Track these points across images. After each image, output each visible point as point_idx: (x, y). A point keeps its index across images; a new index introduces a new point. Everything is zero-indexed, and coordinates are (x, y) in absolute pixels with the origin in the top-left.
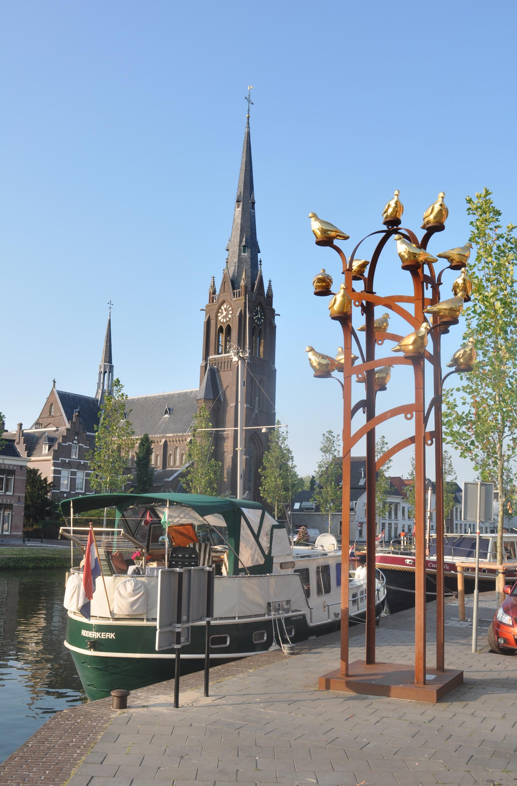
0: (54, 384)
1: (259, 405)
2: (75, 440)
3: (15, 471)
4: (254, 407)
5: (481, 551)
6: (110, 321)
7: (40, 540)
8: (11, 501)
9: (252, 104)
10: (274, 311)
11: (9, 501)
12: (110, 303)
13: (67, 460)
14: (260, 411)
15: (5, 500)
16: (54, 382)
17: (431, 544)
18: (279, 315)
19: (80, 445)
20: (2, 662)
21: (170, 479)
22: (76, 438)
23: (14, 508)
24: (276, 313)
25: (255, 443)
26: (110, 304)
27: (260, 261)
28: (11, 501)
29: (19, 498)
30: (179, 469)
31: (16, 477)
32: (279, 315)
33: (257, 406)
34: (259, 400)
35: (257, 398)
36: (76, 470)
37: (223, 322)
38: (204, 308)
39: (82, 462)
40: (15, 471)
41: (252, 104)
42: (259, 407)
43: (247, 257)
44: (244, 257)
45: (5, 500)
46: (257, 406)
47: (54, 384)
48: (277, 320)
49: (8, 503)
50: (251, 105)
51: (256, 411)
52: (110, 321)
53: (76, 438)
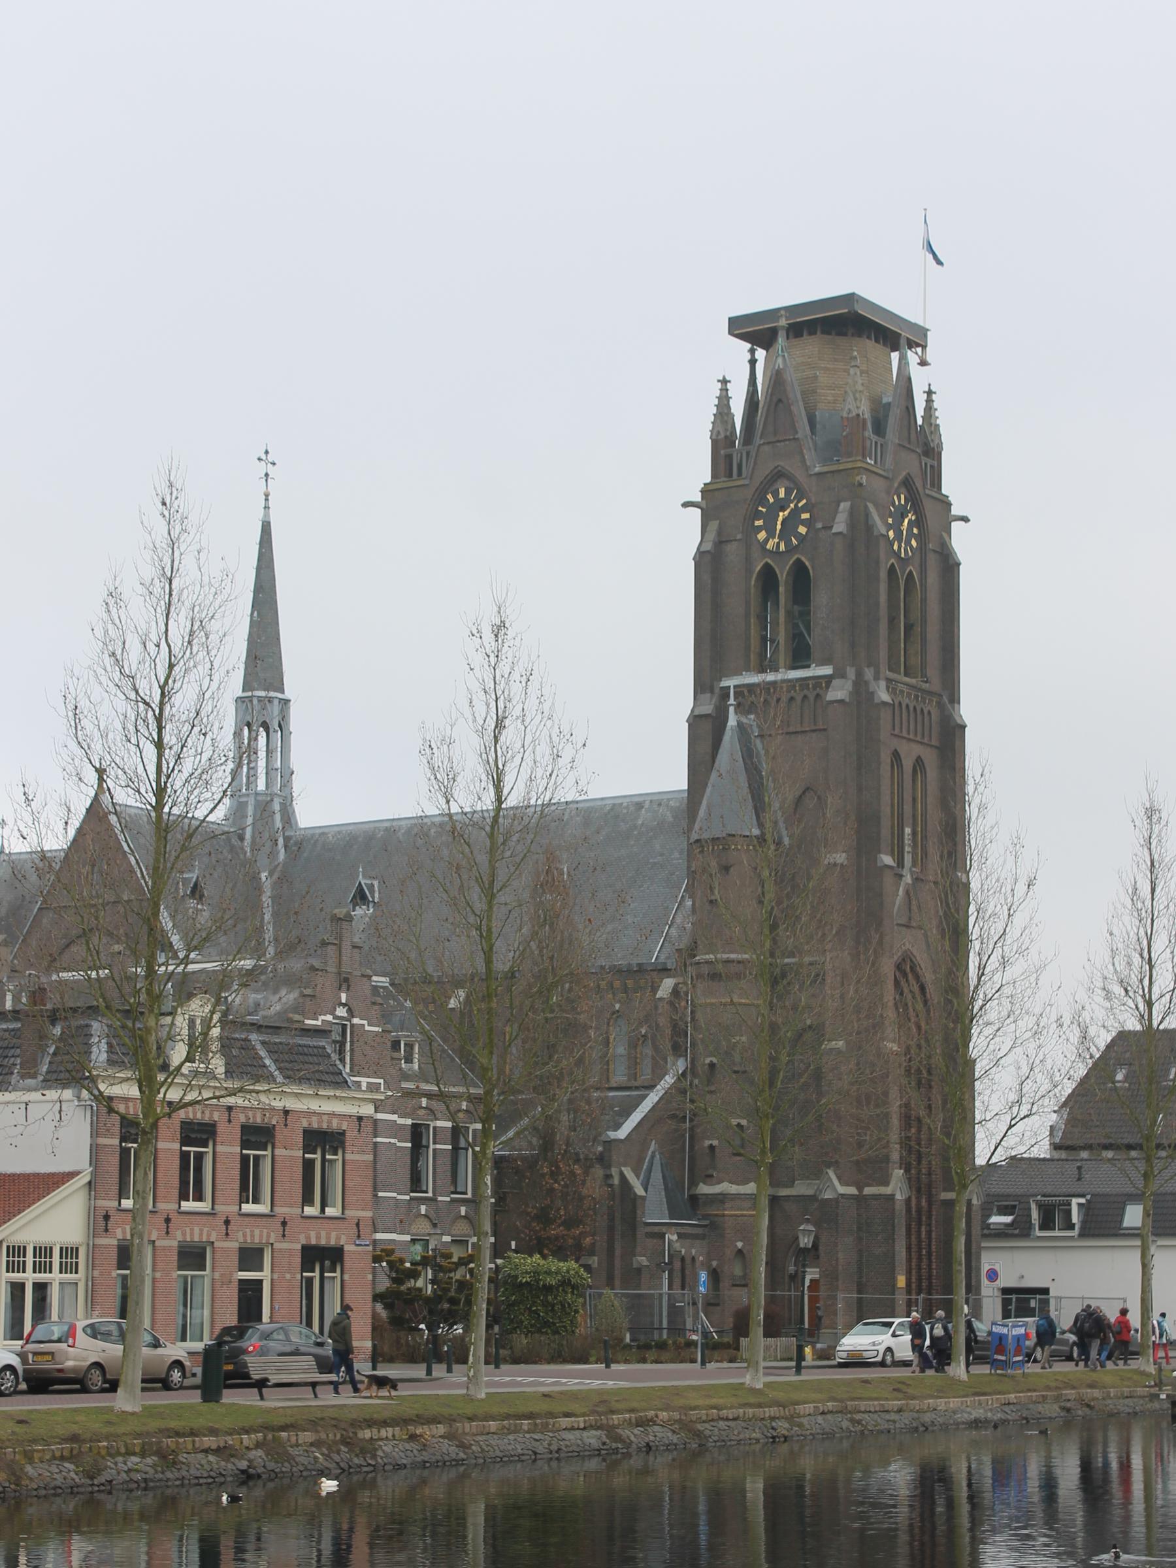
1: (914, 854)
3: (343, 1133)
5: (593, 1359)
6: (266, 529)
8: (338, 1238)
14: (917, 880)
18: (965, 519)
19: (356, 1021)
21: (622, 1133)
22: (343, 997)
23: (347, 1259)
24: (955, 511)
28: (338, 1238)
29: (358, 1225)
30: (348, 1067)
31: (348, 1156)
32: (965, 519)
34: (914, 833)
35: (908, 830)
37: (776, 553)
38: (698, 498)
40: (343, 1133)
45: (313, 1234)
48: (960, 539)
49: (333, 1242)
52: (266, 529)
53: (343, 997)
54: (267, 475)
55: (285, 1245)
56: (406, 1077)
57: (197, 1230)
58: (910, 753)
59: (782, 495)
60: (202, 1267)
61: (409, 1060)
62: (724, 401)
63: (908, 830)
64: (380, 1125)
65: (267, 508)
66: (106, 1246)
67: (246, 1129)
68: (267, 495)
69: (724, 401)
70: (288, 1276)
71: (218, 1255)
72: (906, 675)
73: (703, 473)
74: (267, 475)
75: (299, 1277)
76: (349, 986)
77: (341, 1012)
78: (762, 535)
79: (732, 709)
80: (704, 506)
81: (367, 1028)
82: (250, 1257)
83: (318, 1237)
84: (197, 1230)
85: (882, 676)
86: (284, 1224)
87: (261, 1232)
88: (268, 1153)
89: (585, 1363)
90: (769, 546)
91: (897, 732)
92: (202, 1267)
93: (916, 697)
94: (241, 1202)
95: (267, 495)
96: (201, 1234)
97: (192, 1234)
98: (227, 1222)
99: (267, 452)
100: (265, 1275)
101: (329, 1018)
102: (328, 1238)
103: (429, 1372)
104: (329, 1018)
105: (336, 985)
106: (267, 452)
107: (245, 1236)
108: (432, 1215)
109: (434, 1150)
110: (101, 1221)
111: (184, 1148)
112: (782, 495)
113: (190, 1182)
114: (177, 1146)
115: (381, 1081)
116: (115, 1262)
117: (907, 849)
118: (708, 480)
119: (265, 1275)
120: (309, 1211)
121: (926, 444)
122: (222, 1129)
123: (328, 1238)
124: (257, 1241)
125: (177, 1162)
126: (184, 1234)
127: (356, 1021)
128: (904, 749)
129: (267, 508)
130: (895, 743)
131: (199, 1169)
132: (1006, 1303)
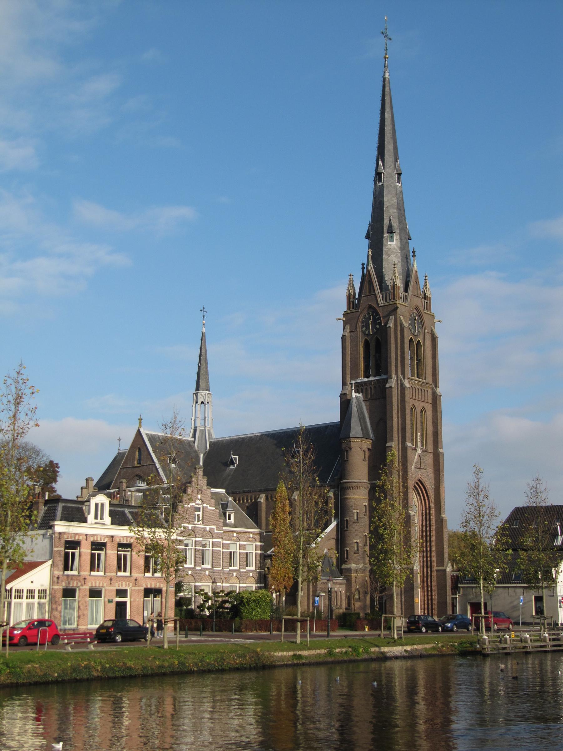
0: (140, 423)
1: (422, 442)
2: (198, 499)
4: (417, 446)
7: (199, 633)
9: (390, 39)
10: (433, 316)
11: (158, 584)
12: (203, 310)
13: (190, 526)
14: (423, 451)
15: (153, 583)
16: (140, 420)
17: (80, 599)
19: (205, 505)
20: (424, 745)
25: (419, 493)
26: (204, 311)
27: (414, 252)
28: (160, 585)
33: (419, 444)
34: (422, 435)
35: (419, 434)
36: (245, 543)
39: (208, 528)
41: (390, 39)
42: (422, 445)
43: (396, 247)
44: (392, 247)
45: (153, 583)
46: (419, 444)
47: (140, 423)
50: (388, 41)
51: (419, 451)
53: (199, 497)
54: (204, 316)
55: (136, 588)
56: (226, 525)
57: (97, 583)
58: (419, 406)
60: (101, 597)
61: (229, 519)
62: (351, 283)
63: (419, 434)
64: (214, 543)
66: (86, 589)
67: (93, 544)
69: (351, 283)
70: (137, 600)
71: (107, 591)
72: (418, 377)
73: (345, 309)
74: (204, 316)
75: (142, 600)
77: (199, 502)
80: (344, 319)
81: (209, 508)
82: (121, 593)
83: (151, 585)
84: (97, 583)
85: (406, 377)
86: (136, 580)
87: (126, 583)
88: (104, 552)
89: (356, 630)
91: (414, 397)
92: (101, 597)
93: (422, 385)
94: (145, 573)
96: (99, 584)
97: (95, 584)
98: (111, 579)
99: (204, 308)
100: (128, 600)
102: (155, 585)
103: (328, 633)
104: (193, 504)
106: (204, 308)
107: (118, 584)
108: (238, 576)
109: (213, 550)
110: (55, 580)
111: (147, 554)
113: (94, 564)
114: (89, 551)
115: (215, 527)
116: (88, 595)
117: (419, 440)
118: (346, 310)
119: (128, 600)
120: (147, 575)
121: (425, 295)
122: (108, 545)
123: (155, 585)
124: (97, 586)
125: (89, 557)
126: (92, 584)
127: (205, 505)
130: (412, 402)
131: (99, 559)
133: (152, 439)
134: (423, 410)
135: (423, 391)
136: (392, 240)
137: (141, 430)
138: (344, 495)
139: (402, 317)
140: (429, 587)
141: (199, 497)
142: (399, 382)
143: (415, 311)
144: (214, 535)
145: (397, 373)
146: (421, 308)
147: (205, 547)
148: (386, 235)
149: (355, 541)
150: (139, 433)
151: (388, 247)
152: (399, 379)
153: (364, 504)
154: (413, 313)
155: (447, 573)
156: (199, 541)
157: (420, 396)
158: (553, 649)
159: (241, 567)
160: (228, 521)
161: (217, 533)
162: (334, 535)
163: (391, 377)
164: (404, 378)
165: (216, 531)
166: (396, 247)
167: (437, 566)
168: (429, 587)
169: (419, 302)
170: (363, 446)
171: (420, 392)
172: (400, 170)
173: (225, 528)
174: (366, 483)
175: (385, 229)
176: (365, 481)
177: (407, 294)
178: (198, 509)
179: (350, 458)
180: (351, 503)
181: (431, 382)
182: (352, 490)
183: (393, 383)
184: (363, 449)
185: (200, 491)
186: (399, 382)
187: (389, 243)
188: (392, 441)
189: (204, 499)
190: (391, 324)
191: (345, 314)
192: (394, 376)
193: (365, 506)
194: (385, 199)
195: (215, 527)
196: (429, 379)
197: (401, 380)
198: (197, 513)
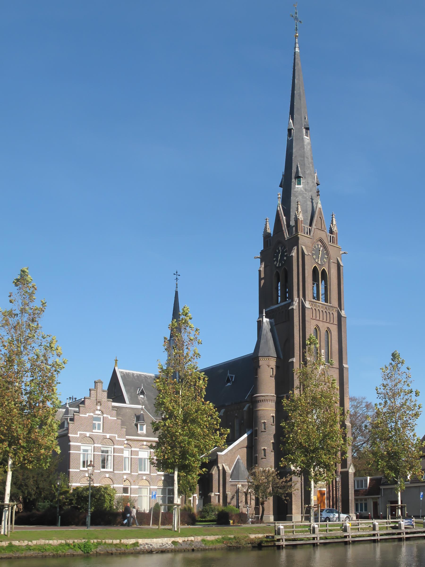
0: (116, 363)
6: (177, 293)
19: (105, 415)
39: (108, 436)
47: (116, 363)
52: (177, 293)
54: (177, 278)
59: (325, 260)
64: (115, 450)
65: (177, 287)
68: (177, 284)
73: (262, 248)
74: (177, 278)
76: (101, 404)
78: (275, 263)
79: (264, 316)
81: (109, 416)
90: (277, 265)
93: (326, 308)
95: (177, 284)
99: (177, 272)
101: (92, 414)
104: (92, 414)
105: (95, 403)
106: (177, 272)
112: (325, 260)
115: (116, 435)
127: (105, 415)
128: (320, 324)
129: (177, 287)
132: (155, 524)
133: (124, 376)
134: (328, 331)
135: (332, 315)
136: (299, 184)
137: (116, 368)
138: (256, 407)
139: (303, 247)
140: (334, 486)
141: (99, 408)
142: (301, 305)
143: (320, 243)
144: (115, 442)
145: (298, 297)
146: (326, 241)
147: (108, 453)
148: (293, 180)
149: (263, 448)
150: (114, 372)
151: (296, 190)
152: (301, 301)
153: (272, 415)
154: (318, 245)
155: (350, 474)
156: (98, 447)
157: (325, 318)
158: (322, 541)
159: (151, 471)
160: (139, 432)
161: (118, 440)
162: (246, 444)
163: (292, 300)
164: (305, 301)
165: (117, 439)
166: (302, 189)
167: (341, 468)
168: (334, 486)
169: (325, 235)
170: (270, 364)
171: (325, 314)
172: (308, 125)
173: (127, 437)
174: (273, 396)
175: (293, 175)
176: (272, 395)
177: (310, 228)
178: (98, 419)
179: (259, 374)
180: (260, 413)
181: (337, 305)
182: (260, 403)
183: (295, 305)
184: (271, 367)
185: (99, 402)
186: (301, 305)
187: (297, 186)
188: (293, 357)
189: (103, 410)
190: (294, 254)
191: (262, 253)
192: (296, 299)
193: (273, 416)
194: (294, 150)
195: (116, 435)
196: (334, 302)
197: (302, 302)
198: (97, 423)
